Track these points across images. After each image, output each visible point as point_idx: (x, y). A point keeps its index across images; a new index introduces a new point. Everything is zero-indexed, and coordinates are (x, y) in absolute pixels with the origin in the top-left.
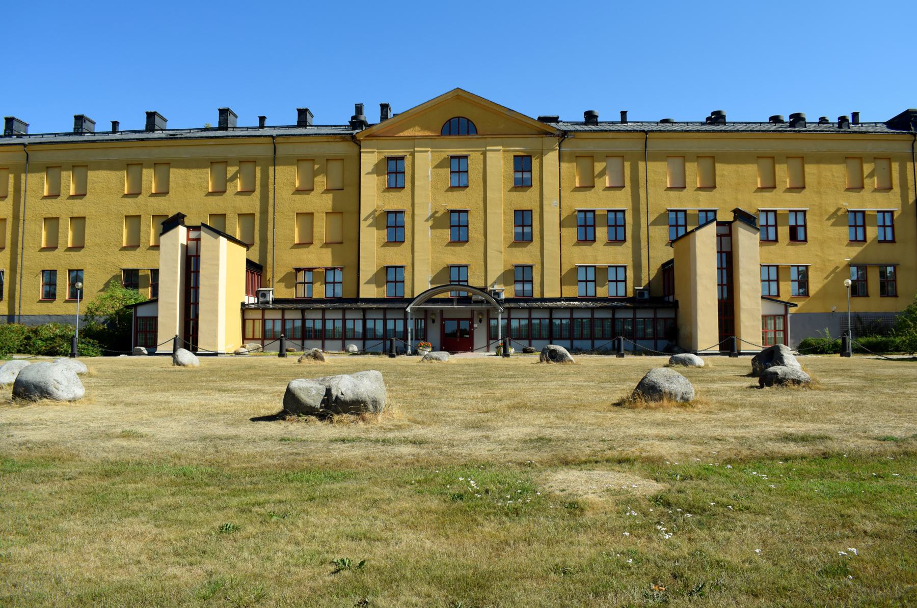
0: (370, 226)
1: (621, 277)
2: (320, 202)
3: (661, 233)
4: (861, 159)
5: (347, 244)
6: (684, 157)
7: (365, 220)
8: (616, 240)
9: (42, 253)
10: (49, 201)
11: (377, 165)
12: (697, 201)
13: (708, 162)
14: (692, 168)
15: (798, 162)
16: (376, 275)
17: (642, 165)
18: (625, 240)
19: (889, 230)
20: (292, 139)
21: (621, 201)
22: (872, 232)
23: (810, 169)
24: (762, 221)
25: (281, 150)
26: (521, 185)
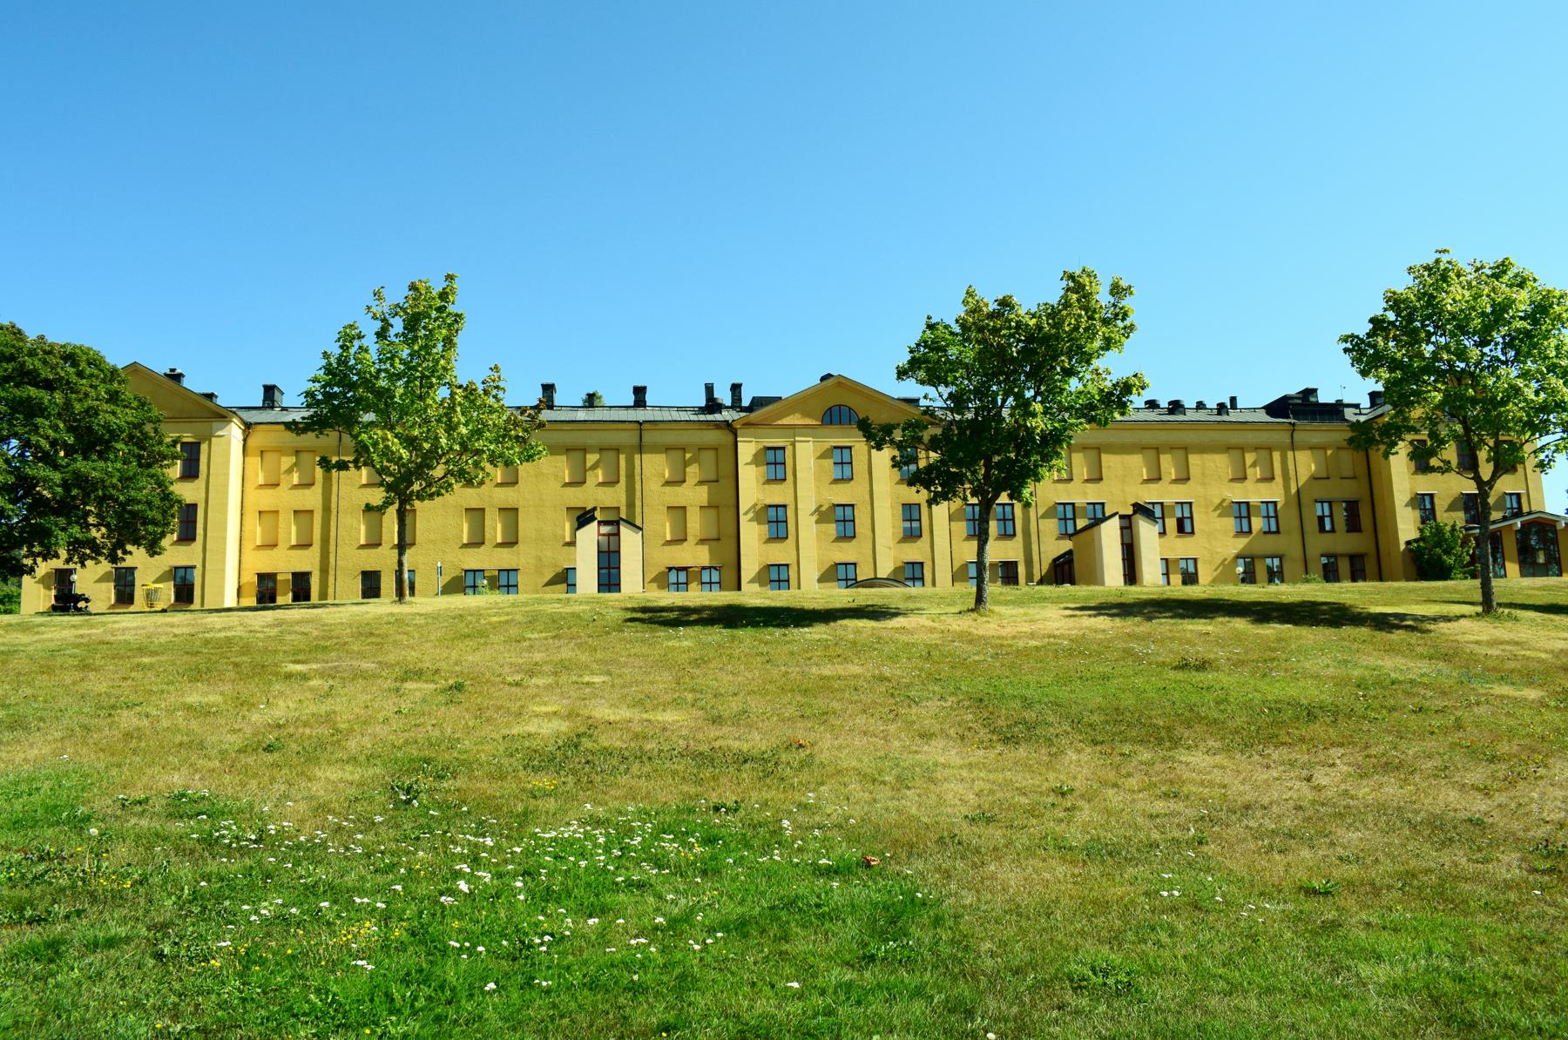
1: (918, 575)
2: (694, 495)
3: (1051, 527)
4: (1242, 449)
5: (726, 540)
11: (756, 456)
12: (1085, 494)
13: (1094, 453)
17: (1290, 454)
19: (1273, 521)
20: (661, 426)
22: (1258, 523)
23: (1194, 459)
25: (647, 437)
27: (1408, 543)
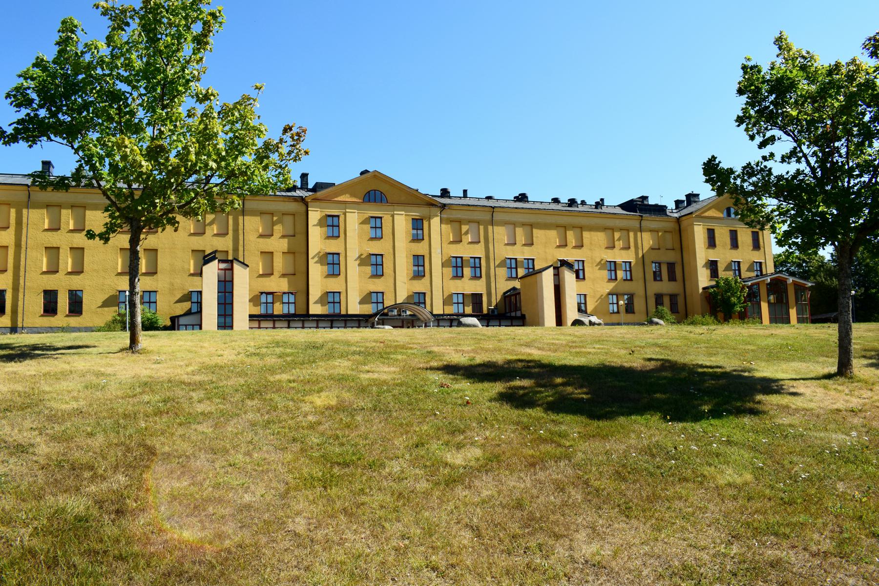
0: (316, 262)
1: (337, 300)
2: (278, 244)
3: (503, 272)
4: (613, 230)
6: (515, 225)
7: (313, 258)
8: (476, 277)
9: (44, 276)
10: (50, 233)
11: (320, 220)
14: (617, 235)
15: (579, 230)
16: (321, 297)
17: (490, 228)
18: (481, 277)
19: (628, 273)
21: (478, 251)
22: (620, 274)
24: (576, 267)
26: (417, 239)
27: (704, 289)
